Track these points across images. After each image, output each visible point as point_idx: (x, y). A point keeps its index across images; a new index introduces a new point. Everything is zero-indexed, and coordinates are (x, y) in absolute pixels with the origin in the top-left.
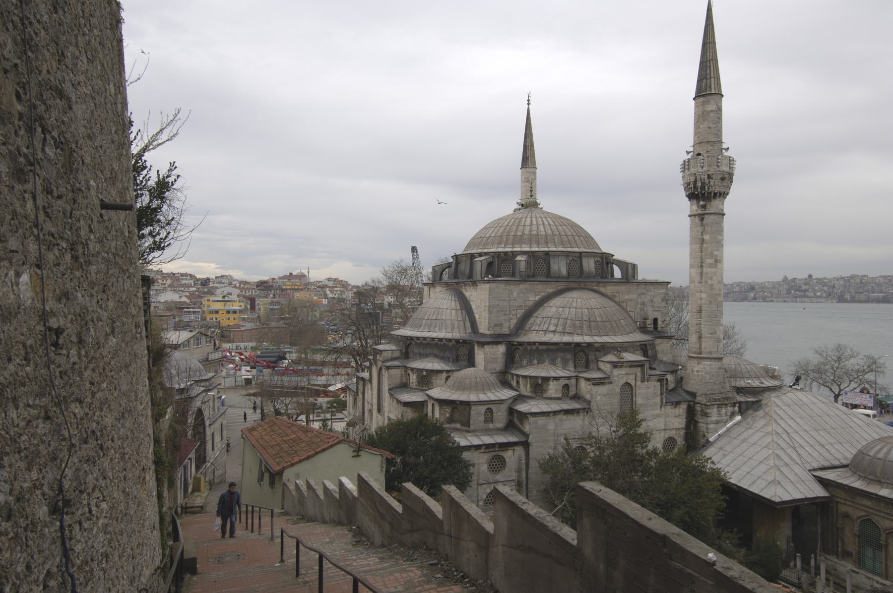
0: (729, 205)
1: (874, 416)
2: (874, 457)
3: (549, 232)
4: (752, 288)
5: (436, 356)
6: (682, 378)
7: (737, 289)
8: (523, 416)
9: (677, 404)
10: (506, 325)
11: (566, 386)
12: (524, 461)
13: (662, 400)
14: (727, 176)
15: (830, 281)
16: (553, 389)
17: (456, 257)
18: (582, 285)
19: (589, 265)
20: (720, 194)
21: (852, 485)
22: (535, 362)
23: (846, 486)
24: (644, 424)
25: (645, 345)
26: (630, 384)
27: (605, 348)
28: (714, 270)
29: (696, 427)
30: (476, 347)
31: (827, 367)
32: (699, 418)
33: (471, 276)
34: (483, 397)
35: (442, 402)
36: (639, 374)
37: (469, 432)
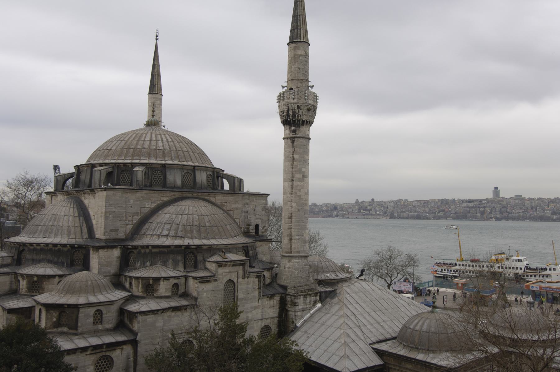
0: (314, 131)
1: (413, 298)
2: (413, 329)
3: (167, 147)
4: (335, 208)
5: (50, 262)
6: (276, 274)
7: (325, 209)
8: (133, 315)
9: (272, 296)
10: (122, 230)
11: (176, 286)
12: (132, 359)
13: (259, 293)
14: (311, 108)
15: (385, 203)
16: (164, 288)
17: (78, 167)
18: (195, 195)
19: (202, 178)
20: (307, 122)
21: (399, 353)
22: (148, 264)
23: (395, 354)
24: (242, 316)
25: (247, 247)
26: (233, 281)
27: (212, 250)
28: (302, 183)
29: (287, 315)
30: (91, 252)
31: (383, 264)
32: (289, 307)
33: (90, 185)
34: (93, 299)
35: (49, 307)
36: (241, 272)
37: (76, 334)
